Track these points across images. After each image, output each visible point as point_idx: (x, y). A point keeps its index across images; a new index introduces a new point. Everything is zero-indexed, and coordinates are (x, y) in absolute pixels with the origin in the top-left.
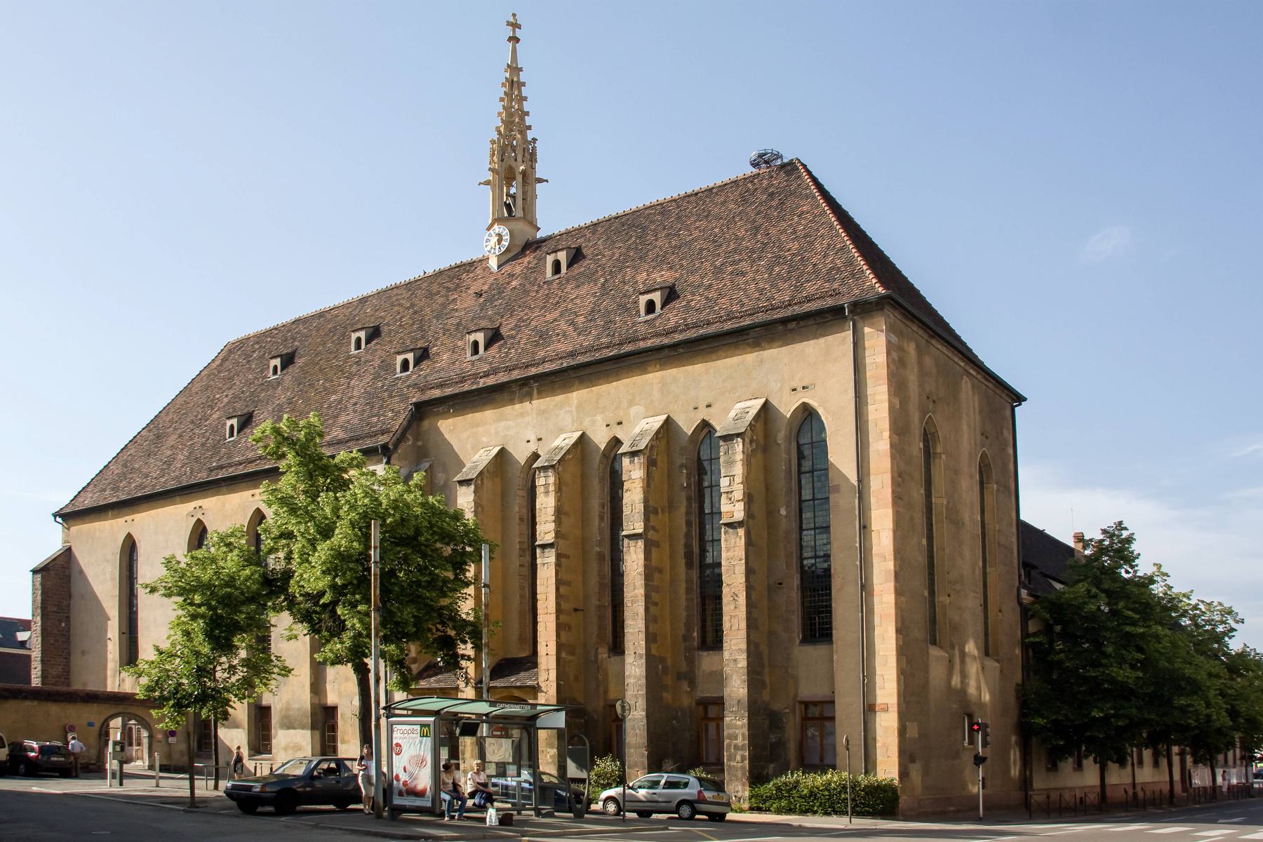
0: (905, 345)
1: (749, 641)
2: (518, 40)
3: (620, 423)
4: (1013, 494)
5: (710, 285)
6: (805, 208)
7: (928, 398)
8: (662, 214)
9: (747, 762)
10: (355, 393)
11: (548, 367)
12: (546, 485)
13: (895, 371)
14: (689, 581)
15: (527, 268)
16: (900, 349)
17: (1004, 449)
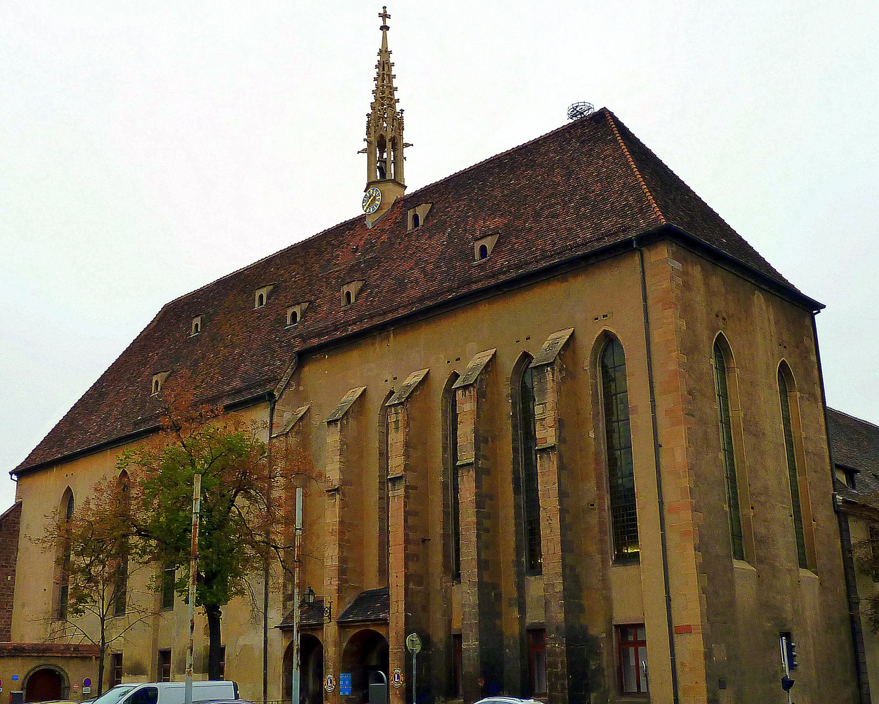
0: (690, 270)
1: (564, 566)
2: (387, 28)
3: (458, 359)
4: (820, 400)
5: (531, 229)
6: (608, 152)
7: (717, 316)
8: (499, 166)
9: (567, 691)
10: (254, 346)
11: (402, 312)
12: (397, 422)
13: (680, 295)
14: (517, 506)
15: (395, 223)
16: (685, 273)
17: (806, 357)
